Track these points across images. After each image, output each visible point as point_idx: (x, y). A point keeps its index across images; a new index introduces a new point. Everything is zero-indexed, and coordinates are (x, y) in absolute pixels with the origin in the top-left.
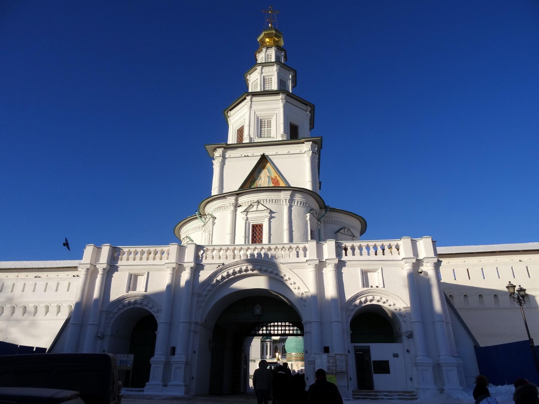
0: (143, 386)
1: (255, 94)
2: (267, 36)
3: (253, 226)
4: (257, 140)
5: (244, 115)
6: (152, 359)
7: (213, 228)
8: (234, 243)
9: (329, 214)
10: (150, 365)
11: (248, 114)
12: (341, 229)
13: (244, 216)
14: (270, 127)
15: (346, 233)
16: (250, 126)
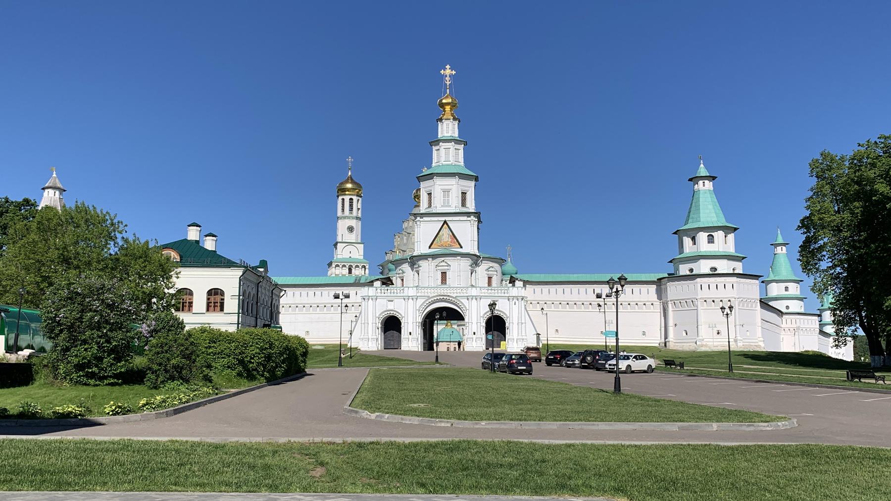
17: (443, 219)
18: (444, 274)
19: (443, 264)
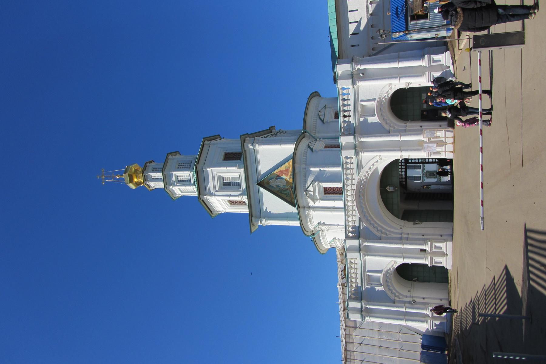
0: (447, 270)
1: (199, 193)
2: (131, 181)
3: (325, 194)
4: (244, 186)
5: (218, 201)
6: (429, 265)
7: (328, 225)
8: (342, 208)
9: (308, 129)
10: (433, 266)
11: (218, 198)
12: (320, 118)
13: (318, 202)
15: (322, 113)
16: (230, 196)
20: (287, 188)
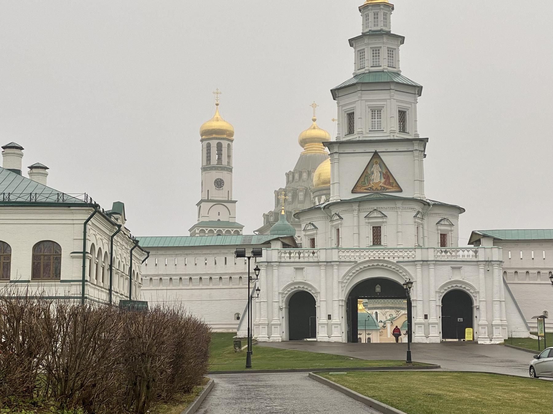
14: (380, 118)
17: (372, 149)
18: (377, 232)
19: (375, 214)
20: (371, 182)
